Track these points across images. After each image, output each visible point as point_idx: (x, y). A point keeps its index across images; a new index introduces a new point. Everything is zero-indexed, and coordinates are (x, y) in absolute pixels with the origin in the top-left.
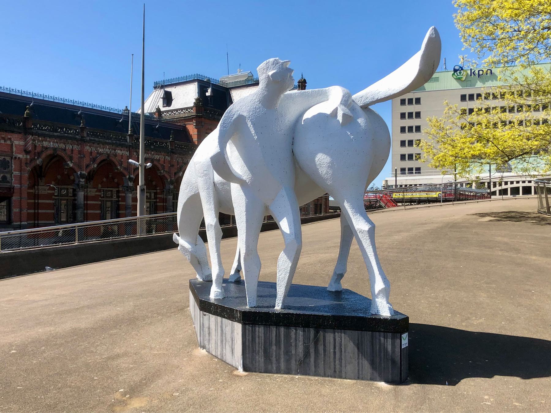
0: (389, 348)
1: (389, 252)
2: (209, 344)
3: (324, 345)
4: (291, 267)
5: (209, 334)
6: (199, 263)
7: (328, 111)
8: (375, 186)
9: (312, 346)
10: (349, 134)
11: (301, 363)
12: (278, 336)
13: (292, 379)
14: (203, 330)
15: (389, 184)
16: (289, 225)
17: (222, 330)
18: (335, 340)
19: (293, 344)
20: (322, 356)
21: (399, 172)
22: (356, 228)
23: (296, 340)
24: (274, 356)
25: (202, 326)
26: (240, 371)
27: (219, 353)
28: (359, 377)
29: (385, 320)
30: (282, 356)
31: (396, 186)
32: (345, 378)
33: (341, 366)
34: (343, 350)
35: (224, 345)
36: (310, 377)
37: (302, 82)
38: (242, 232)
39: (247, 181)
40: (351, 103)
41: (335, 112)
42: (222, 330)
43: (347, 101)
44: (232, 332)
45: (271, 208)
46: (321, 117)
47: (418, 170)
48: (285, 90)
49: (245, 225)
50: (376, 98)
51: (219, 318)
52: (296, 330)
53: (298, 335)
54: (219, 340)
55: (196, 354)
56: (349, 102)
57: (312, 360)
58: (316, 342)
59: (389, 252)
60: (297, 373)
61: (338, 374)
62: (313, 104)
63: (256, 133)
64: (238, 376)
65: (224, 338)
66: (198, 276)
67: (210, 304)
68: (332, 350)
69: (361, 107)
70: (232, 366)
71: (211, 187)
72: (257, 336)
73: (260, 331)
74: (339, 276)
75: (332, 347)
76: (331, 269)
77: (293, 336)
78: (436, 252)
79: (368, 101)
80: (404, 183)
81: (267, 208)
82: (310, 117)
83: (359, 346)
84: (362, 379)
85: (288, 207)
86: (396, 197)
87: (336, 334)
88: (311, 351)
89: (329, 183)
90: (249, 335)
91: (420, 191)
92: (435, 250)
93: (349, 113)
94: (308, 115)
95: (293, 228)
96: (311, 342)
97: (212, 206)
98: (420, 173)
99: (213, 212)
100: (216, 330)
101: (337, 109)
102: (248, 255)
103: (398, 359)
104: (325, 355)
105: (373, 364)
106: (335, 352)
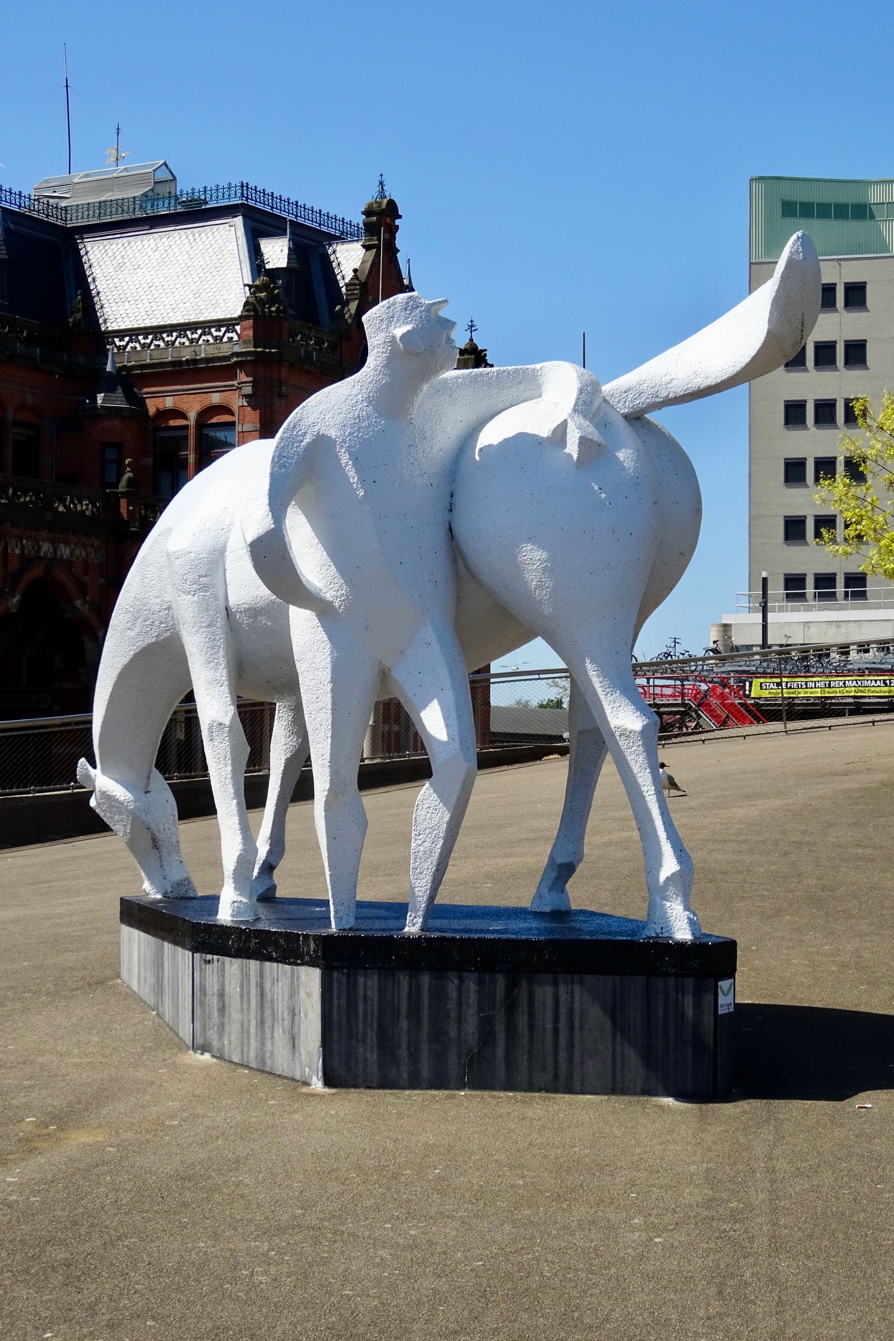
0: (690, 1011)
1: (711, 851)
2: (221, 1038)
3: (531, 1015)
4: (449, 823)
5: (222, 1009)
6: (155, 844)
7: (544, 431)
8: (680, 649)
9: (500, 1015)
10: (596, 488)
11: (471, 1060)
12: (414, 994)
13: (453, 1097)
14: (202, 1004)
15: (738, 640)
16: (446, 718)
17: (262, 995)
18: (556, 999)
19: (453, 1014)
20: (526, 1040)
21: (777, 590)
22: (612, 726)
23: (460, 1003)
24: (404, 1045)
25: (198, 993)
26: (317, 1084)
27: (252, 1054)
28: (615, 1088)
29: (681, 946)
30: (425, 1046)
31: (765, 644)
32: (583, 1092)
33: (570, 1061)
34: (577, 1024)
35: (268, 1031)
36: (495, 1093)
37: (381, 213)
38: (322, 735)
39: (337, 605)
40: (599, 408)
41: (561, 431)
42: (262, 995)
43: (589, 403)
44: (293, 992)
45: (398, 674)
46: (522, 442)
47: (857, 584)
48: (436, 372)
49: (329, 716)
50: (664, 394)
51: (254, 964)
52: (461, 981)
53: (466, 992)
54: (253, 1022)
55: (188, 1062)
56: (595, 406)
57: (500, 1050)
58: (511, 1008)
59: (711, 851)
60: (461, 1086)
61: (563, 1082)
62: (501, 406)
63: (362, 481)
64: (313, 1095)
65: (268, 1012)
66: (147, 886)
67: (224, 931)
68: (549, 1026)
69: (626, 417)
70: (293, 1079)
71: (220, 622)
72: (361, 997)
73: (369, 983)
74: (562, 871)
75: (549, 1016)
76: (539, 857)
77: (452, 993)
78: (860, 851)
79: (640, 402)
80: (798, 638)
81: (384, 676)
82: (495, 442)
83: (615, 1013)
84: (623, 1093)
85: (444, 672)
86: (765, 694)
87: (562, 987)
88: (497, 1029)
89: (547, 610)
90: (339, 994)
91: (861, 672)
92: (858, 846)
93: (596, 436)
94: (493, 434)
95: (454, 722)
96: (497, 1006)
97: (222, 673)
98: (862, 595)
99: (225, 689)
100: (244, 995)
101: (564, 424)
102: (336, 796)
103: (709, 1038)
104: (531, 1038)
105: (648, 1058)
106: (556, 1031)
